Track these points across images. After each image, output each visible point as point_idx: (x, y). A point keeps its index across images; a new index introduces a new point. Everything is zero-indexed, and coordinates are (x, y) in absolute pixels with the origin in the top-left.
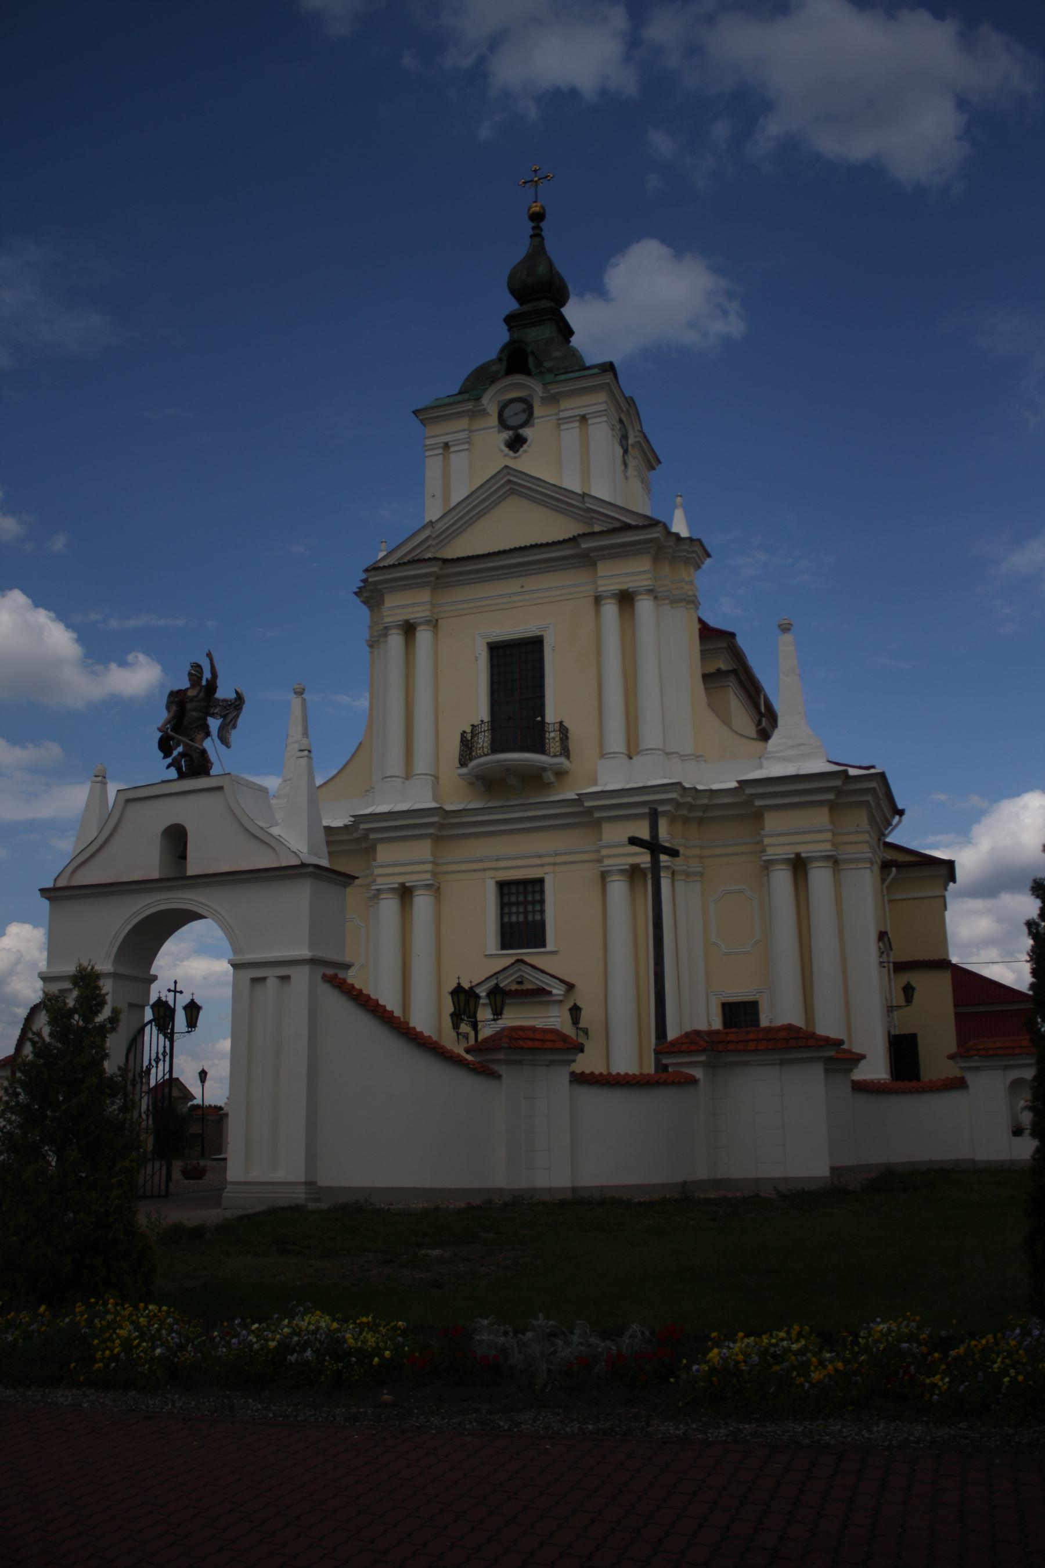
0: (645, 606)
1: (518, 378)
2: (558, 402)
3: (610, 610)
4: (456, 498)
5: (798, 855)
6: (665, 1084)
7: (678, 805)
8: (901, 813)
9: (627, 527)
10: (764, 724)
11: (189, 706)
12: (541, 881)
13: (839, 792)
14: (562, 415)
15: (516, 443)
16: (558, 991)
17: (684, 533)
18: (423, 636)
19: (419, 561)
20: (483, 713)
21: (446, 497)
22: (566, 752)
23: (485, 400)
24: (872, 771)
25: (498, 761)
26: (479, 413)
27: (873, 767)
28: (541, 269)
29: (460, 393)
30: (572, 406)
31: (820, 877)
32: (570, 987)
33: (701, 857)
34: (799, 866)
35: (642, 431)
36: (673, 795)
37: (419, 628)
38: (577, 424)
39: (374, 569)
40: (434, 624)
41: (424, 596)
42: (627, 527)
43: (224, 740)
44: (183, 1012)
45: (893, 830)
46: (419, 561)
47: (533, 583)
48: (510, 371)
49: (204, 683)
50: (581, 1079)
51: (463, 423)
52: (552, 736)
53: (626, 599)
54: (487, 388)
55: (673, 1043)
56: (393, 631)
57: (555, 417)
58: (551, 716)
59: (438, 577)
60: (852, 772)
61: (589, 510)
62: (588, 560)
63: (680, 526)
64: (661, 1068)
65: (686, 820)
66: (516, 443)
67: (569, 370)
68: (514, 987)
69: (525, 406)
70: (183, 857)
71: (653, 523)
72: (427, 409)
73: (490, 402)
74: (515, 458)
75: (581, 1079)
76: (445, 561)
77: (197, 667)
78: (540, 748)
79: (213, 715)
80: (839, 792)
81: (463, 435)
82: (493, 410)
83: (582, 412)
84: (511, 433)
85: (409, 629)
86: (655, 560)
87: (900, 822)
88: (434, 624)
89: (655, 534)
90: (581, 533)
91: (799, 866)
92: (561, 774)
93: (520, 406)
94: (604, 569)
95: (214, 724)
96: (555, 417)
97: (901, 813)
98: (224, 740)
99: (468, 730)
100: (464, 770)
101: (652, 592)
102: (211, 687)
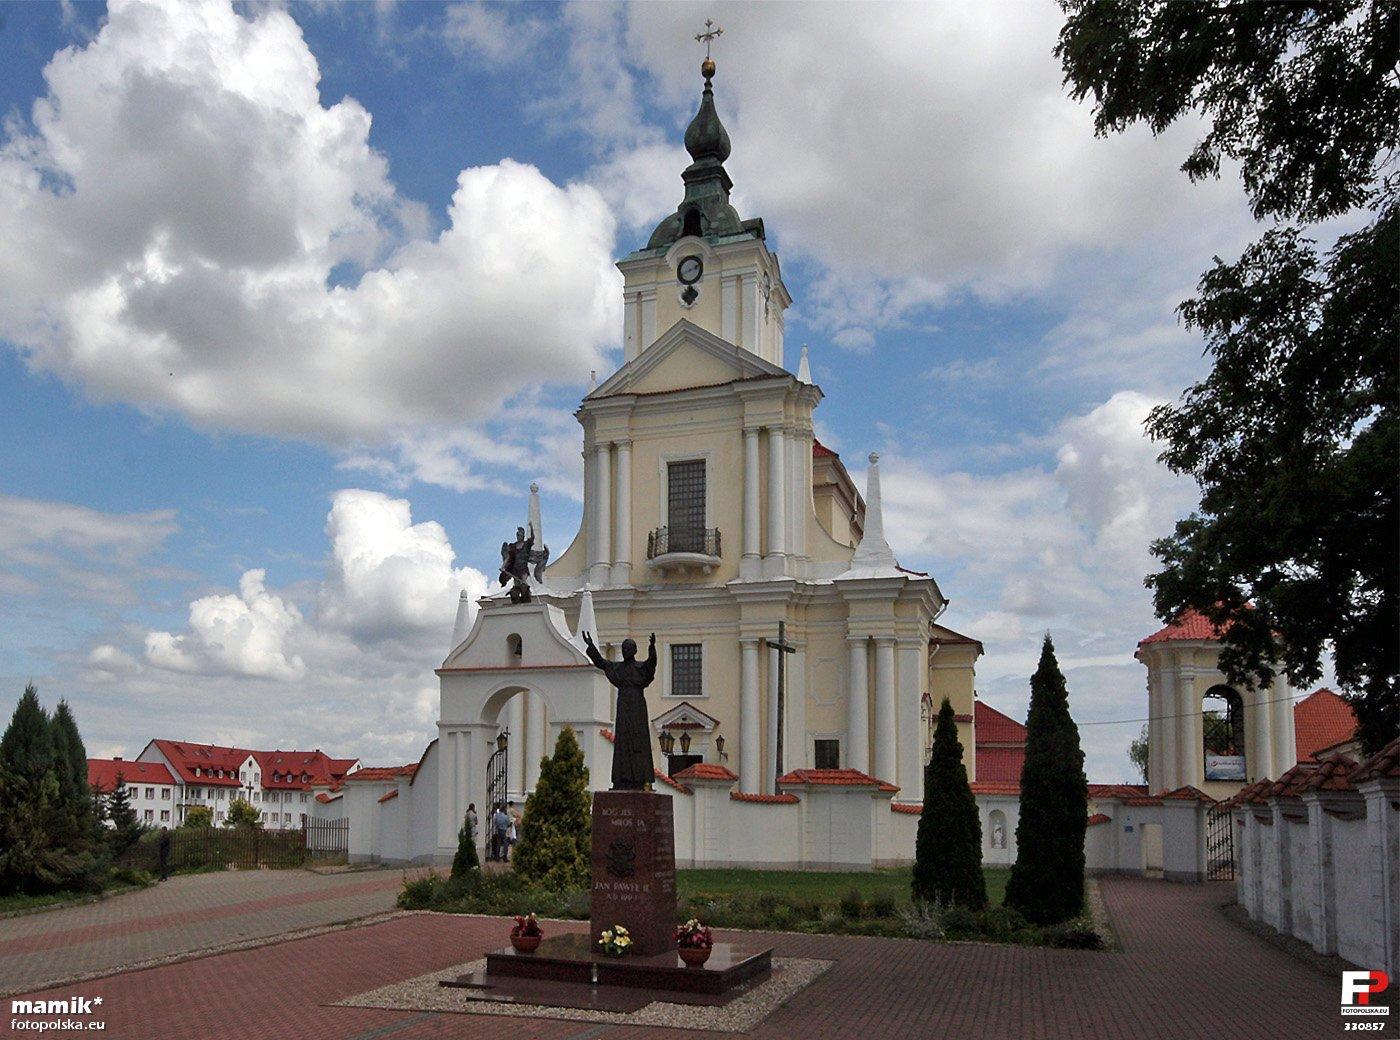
0: (779, 440)
1: (691, 239)
2: (721, 262)
3: (753, 441)
4: (647, 344)
5: (871, 637)
6: (781, 803)
7: (792, 595)
8: (946, 602)
9: (766, 377)
10: (856, 519)
11: (518, 556)
12: (700, 645)
13: (901, 592)
14: (724, 274)
15: (690, 296)
16: (709, 726)
17: (807, 381)
18: (624, 454)
19: (620, 395)
20: (664, 522)
21: (640, 344)
22: (719, 553)
23: (667, 258)
24: (925, 577)
25: (676, 558)
26: (662, 268)
27: (926, 574)
28: (710, 129)
29: (649, 248)
30: (732, 267)
31: (888, 654)
32: (717, 723)
33: (806, 633)
34: (871, 644)
35: (780, 280)
36: (786, 598)
37: (620, 449)
38: (734, 283)
39: (589, 399)
40: (630, 443)
41: (624, 422)
42: (766, 377)
43: (538, 579)
44: (667, 793)
45: (939, 616)
46: (620, 395)
47: (701, 416)
48: (686, 233)
49: (525, 540)
50: (894, 809)
51: (653, 277)
52: (710, 540)
53: (764, 432)
54: (669, 247)
55: (786, 777)
56: (603, 450)
57: (718, 275)
58: (709, 525)
59: (634, 408)
60: (912, 577)
61: (740, 360)
62: (738, 400)
63: (804, 376)
64: (778, 791)
65: (797, 606)
66: (690, 296)
67: (730, 232)
68: (680, 722)
69: (697, 263)
70: (519, 652)
71: (785, 375)
72: (741, 677)
73: (671, 259)
74: (689, 309)
75: (894, 809)
76: (639, 396)
77: (521, 530)
78: (701, 548)
79: (530, 561)
80: (901, 592)
81: (651, 287)
82: (673, 265)
83: (640, 289)
84: (686, 286)
85: (613, 448)
86: (785, 403)
87: (945, 609)
88: (630, 443)
89: (789, 383)
90: (737, 378)
91: (871, 644)
92: (714, 567)
93: (692, 263)
94: (751, 408)
95: (531, 567)
96: (718, 275)
97: (946, 602)
98: (538, 579)
99: (654, 531)
100: (650, 562)
101: (784, 430)
102: (530, 542)
